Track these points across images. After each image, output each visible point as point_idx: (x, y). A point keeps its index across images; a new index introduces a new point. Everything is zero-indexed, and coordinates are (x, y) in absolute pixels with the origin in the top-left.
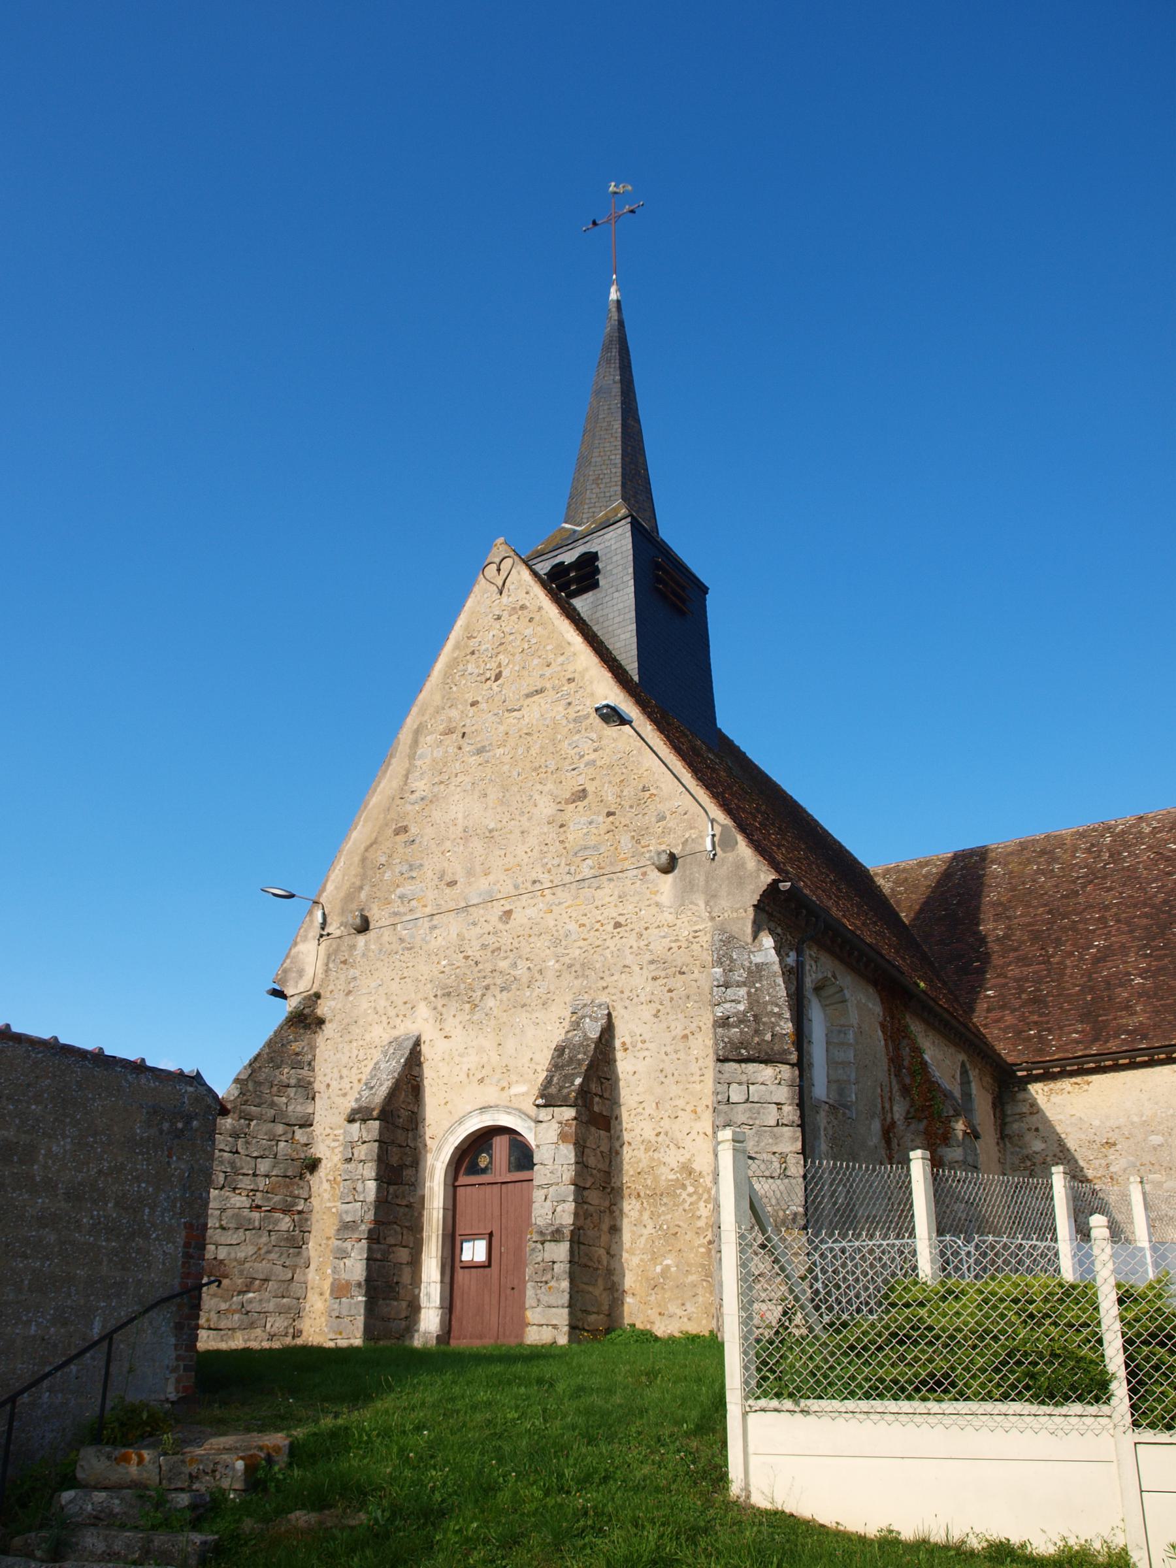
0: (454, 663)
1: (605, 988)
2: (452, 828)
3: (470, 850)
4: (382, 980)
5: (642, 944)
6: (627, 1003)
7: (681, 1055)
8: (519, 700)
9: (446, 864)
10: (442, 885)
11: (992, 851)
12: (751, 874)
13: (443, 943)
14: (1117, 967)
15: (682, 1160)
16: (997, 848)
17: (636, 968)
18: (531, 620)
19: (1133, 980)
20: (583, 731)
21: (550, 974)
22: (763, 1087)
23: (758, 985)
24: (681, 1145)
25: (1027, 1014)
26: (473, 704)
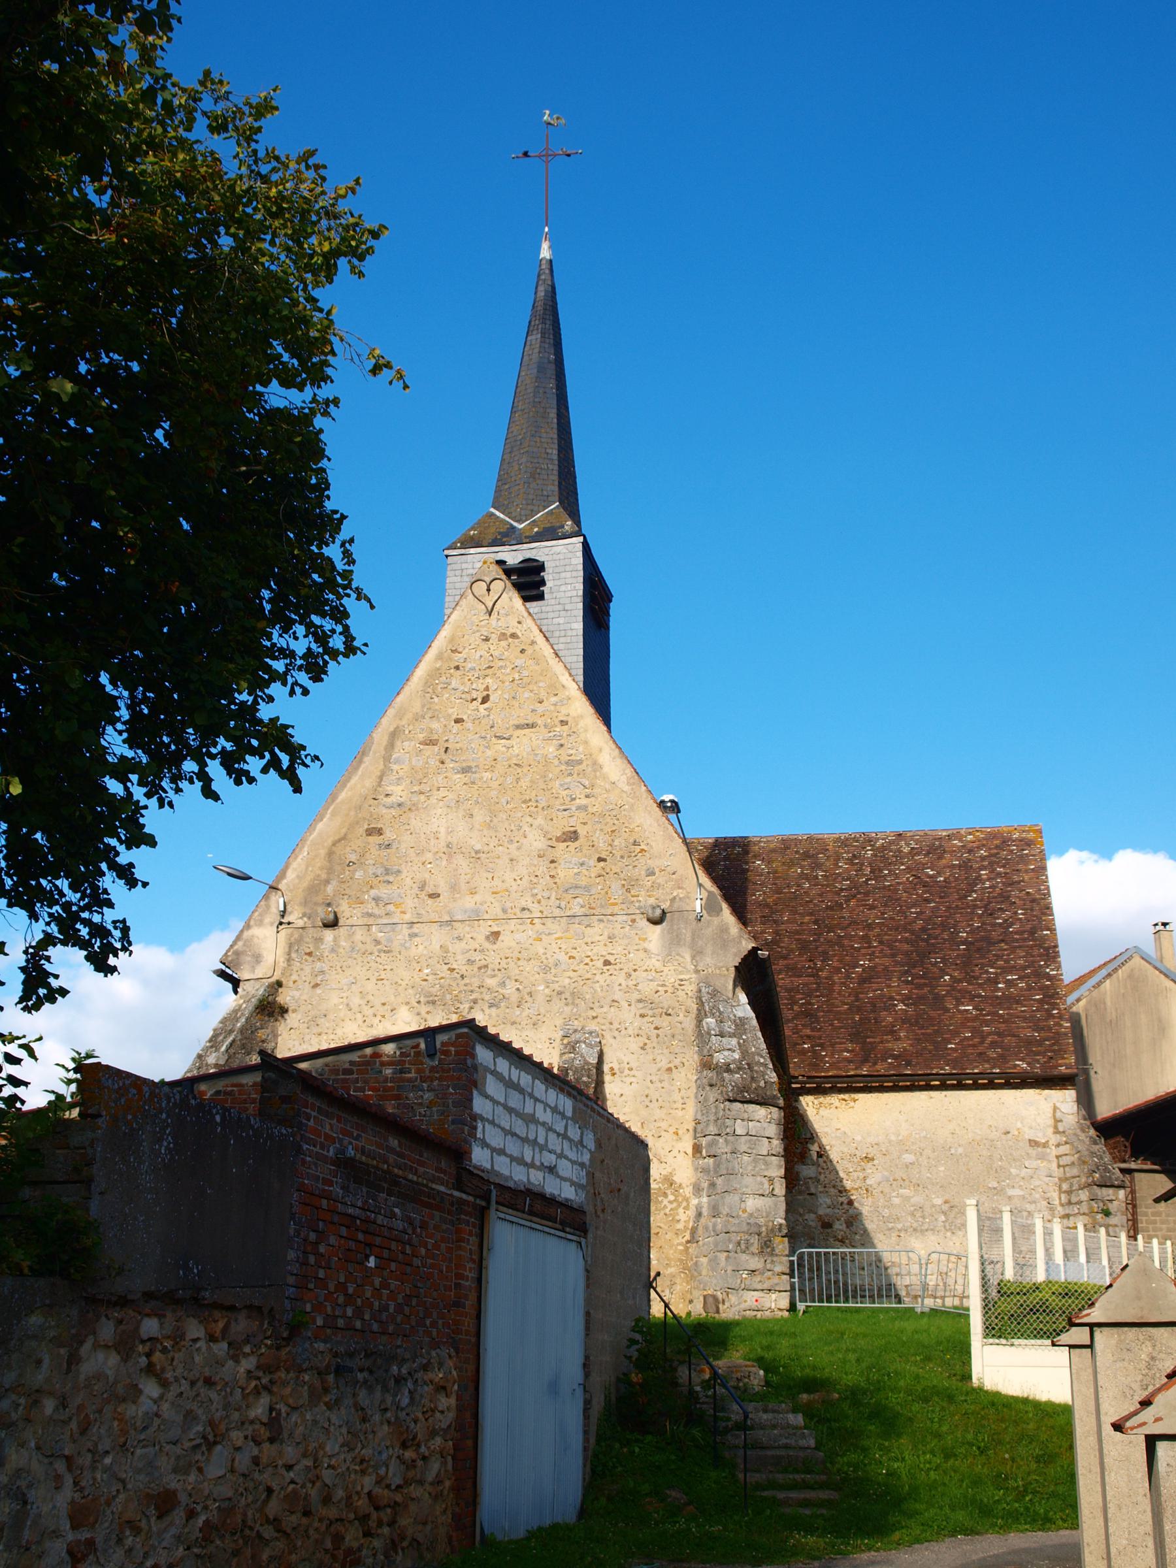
0: (435, 673)
1: (594, 1018)
2: (433, 842)
3: (454, 866)
4: (355, 978)
5: (631, 983)
6: (616, 1033)
7: (665, 1084)
8: (508, 729)
9: (427, 876)
10: (423, 895)
11: (755, 844)
12: (734, 939)
13: (425, 952)
14: (882, 990)
15: (664, 1173)
16: (760, 842)
17: (625, 1004)
18: (522, 651)
19: (896, 1005)
20: (575, 776)
21: (540, 999)
22: (758, 1124)
23: (744, 1037)
24: (663, 1160)
25: (800, 1027)
26: (457, 721)
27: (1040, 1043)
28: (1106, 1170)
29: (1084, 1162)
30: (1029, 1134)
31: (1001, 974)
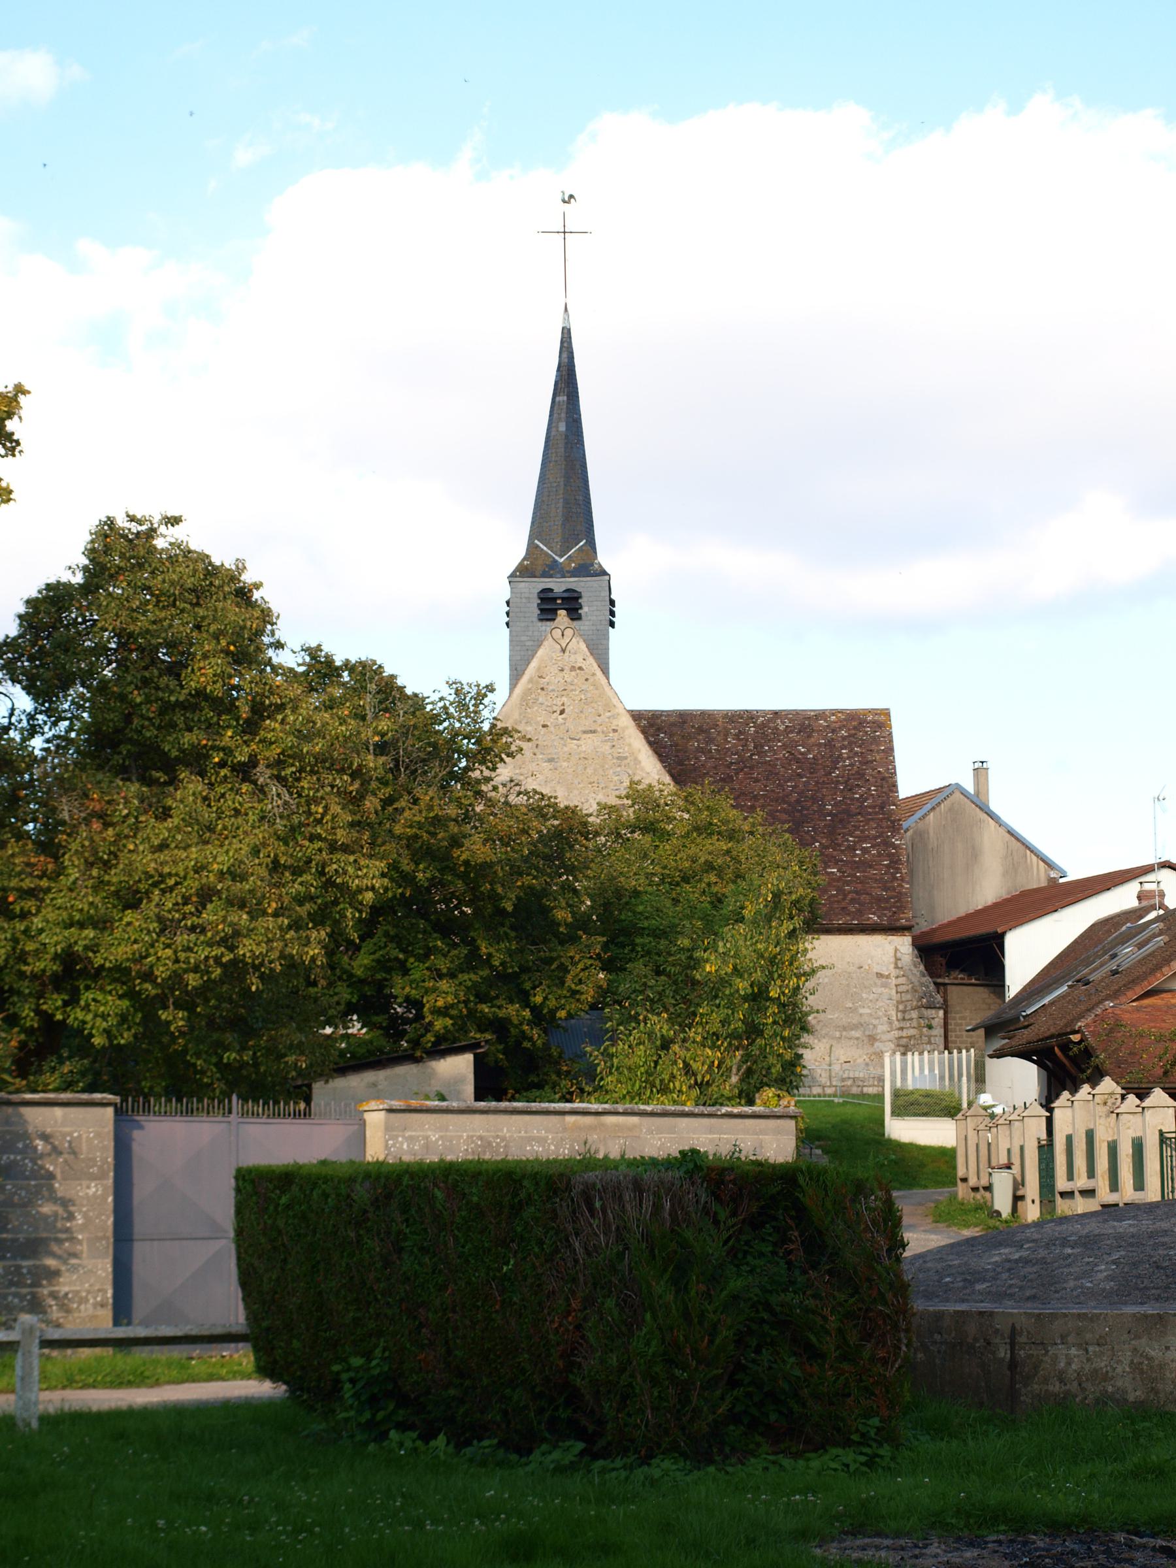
18: (587, 680)
26: (544, 726)
27: (887, 900)
28: (931, 996)
29: (916, 991)
30: (876, 969)
31: (858, 842)
